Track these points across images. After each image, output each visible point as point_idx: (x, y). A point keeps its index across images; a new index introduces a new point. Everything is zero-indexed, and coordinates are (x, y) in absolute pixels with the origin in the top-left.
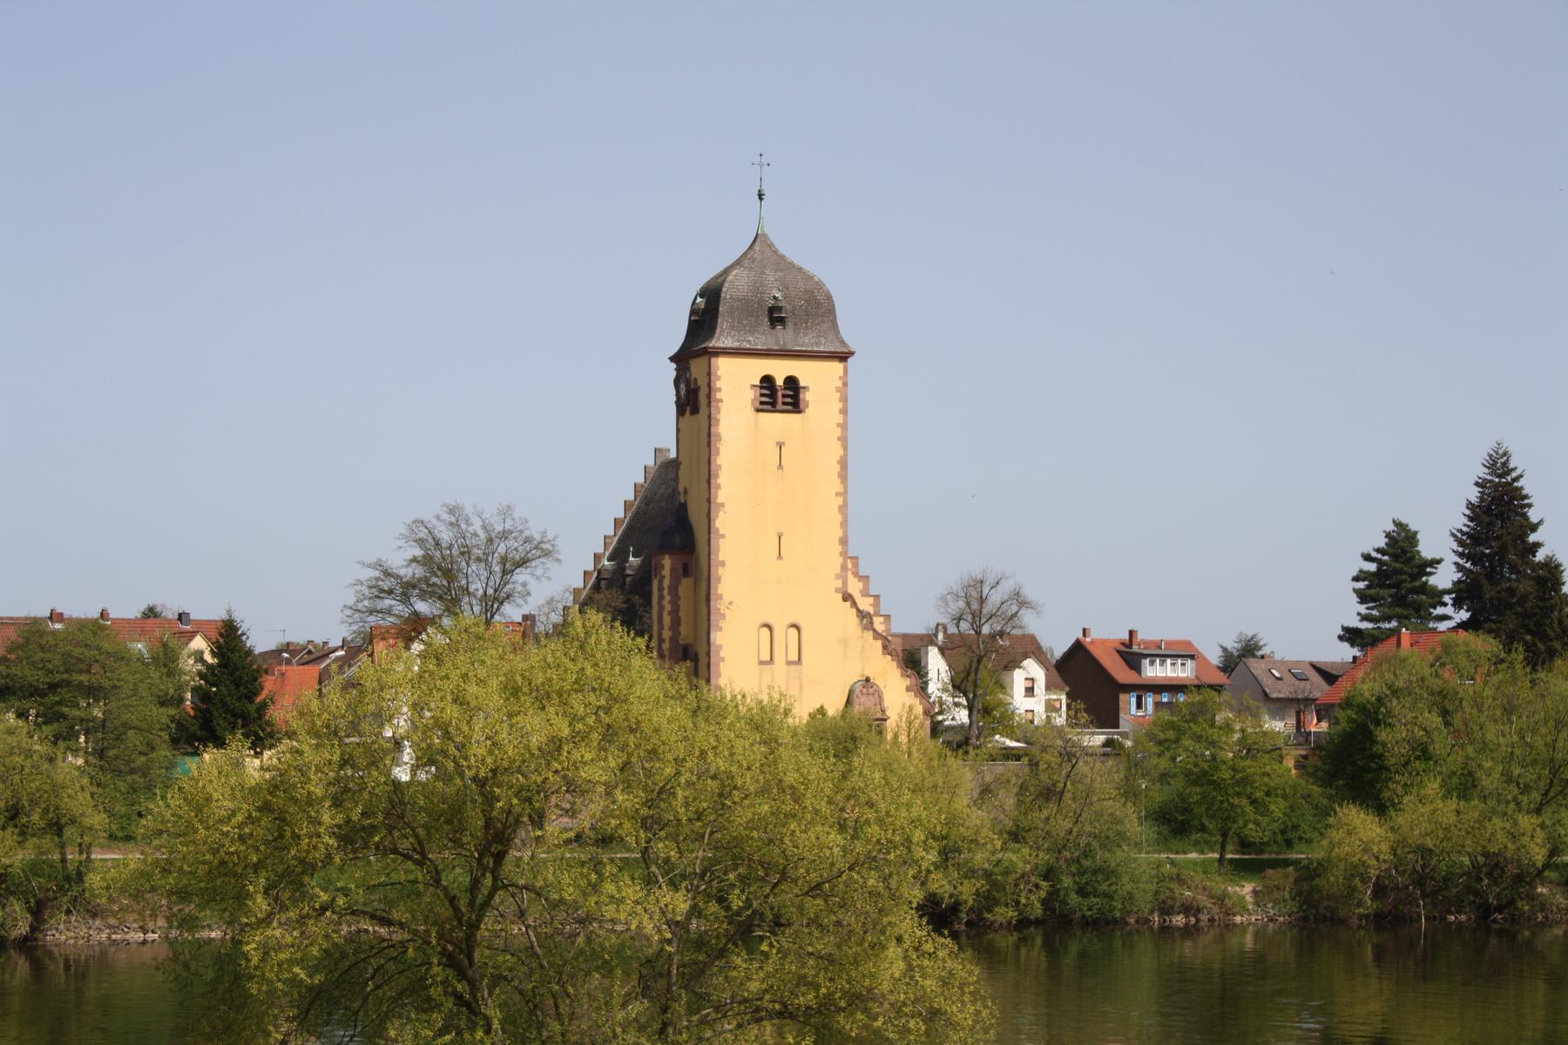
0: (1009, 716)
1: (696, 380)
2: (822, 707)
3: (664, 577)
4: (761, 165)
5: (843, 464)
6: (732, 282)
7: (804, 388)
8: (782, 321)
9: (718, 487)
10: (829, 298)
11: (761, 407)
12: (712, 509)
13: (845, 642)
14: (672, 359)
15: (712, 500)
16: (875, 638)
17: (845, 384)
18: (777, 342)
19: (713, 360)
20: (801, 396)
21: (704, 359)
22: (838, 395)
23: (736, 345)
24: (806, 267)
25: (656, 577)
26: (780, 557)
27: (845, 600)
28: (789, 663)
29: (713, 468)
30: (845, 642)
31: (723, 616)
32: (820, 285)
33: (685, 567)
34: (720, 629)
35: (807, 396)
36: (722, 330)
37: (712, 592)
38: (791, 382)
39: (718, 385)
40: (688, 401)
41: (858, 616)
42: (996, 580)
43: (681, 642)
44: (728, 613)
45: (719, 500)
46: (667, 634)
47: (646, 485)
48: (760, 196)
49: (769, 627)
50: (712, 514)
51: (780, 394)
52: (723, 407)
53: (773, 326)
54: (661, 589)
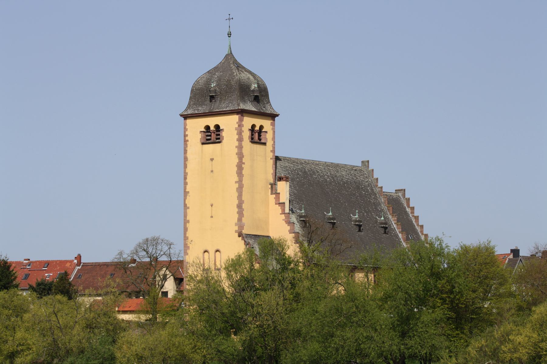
2: (378, 178)
22: (236, 132)
27: (239, 236)
35: (224, 134)
38: (217, 127)
41: (244, 244)
44: (190, 246)
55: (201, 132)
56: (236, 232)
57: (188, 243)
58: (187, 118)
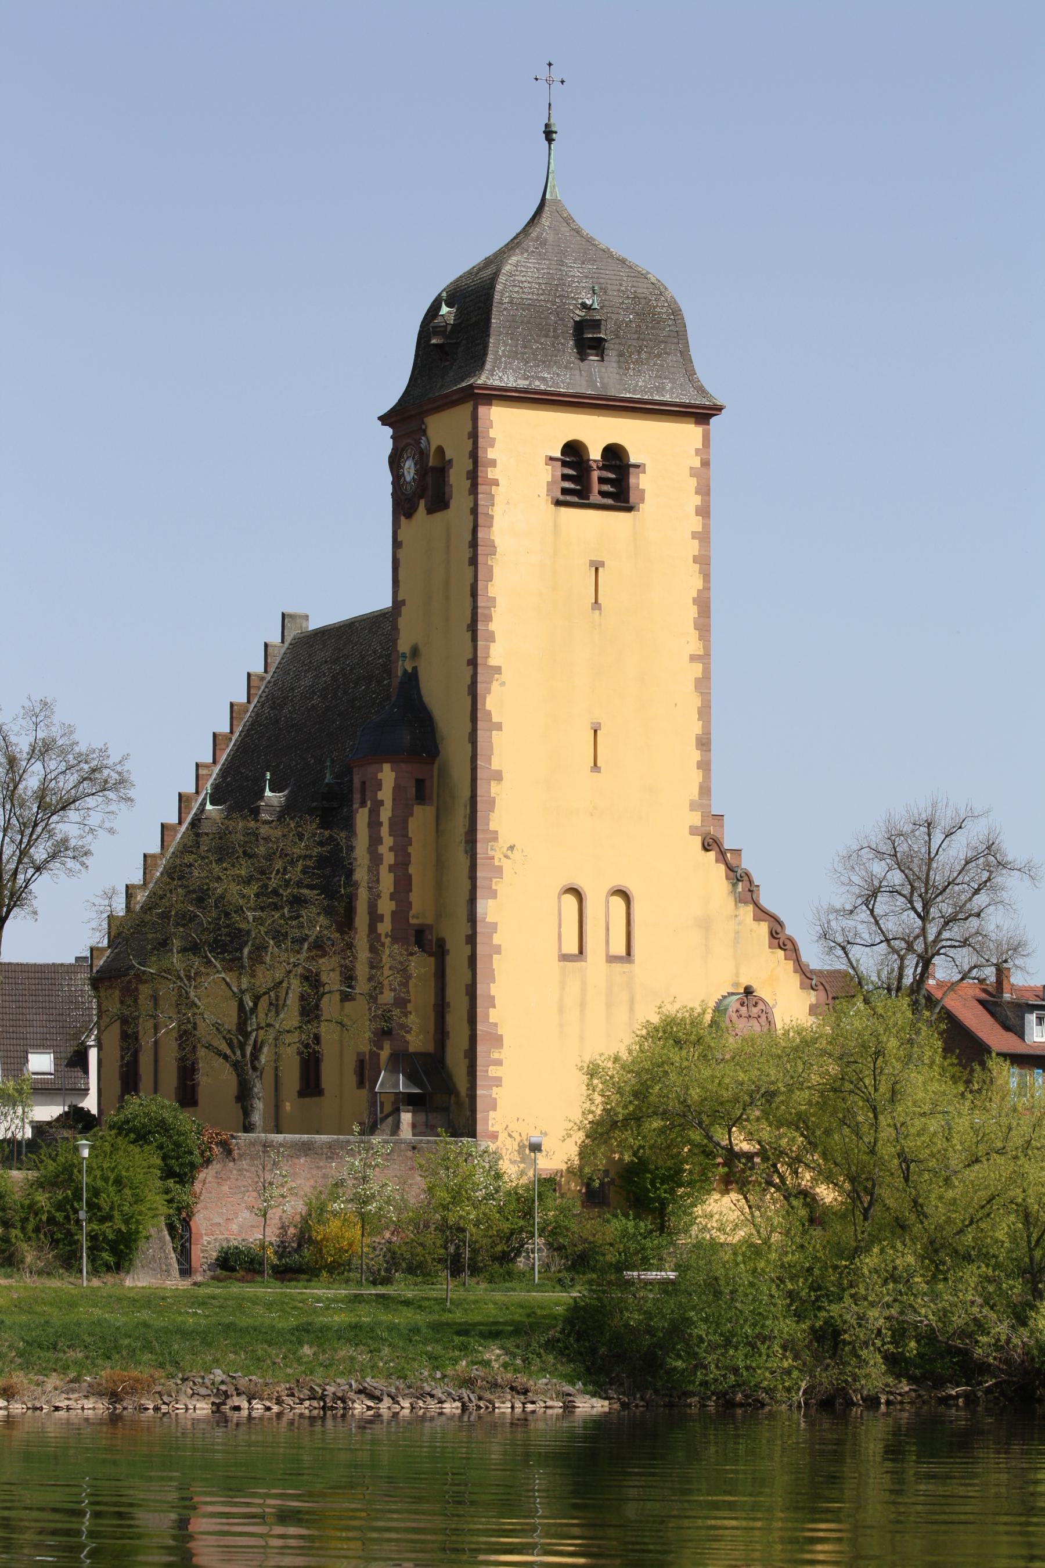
0: (970, 1060)
1: (440, 450)
3: (381, 803)
4: (549, 82)
5: (703, 604)
6: (511, 274)
7: (637, 466)
8: (598, 346)
9: (491, 637)
10: (676, 313)
11: (562, 498)
12: (480, 678)
13: (705, 925)
14: (385, 420)
15: (479, 661)
16: (756, 919)
17: (706, 463)
18: (591, 382)
19: (482, 410)
20: (632, 481)
21: (468, 407)
22: (693, 482)
23: (522, 384)
24: (632, 258)
25: (363, 804)
26: (595, 766)
27: (706, 848)
28: (612, 959)
29: (481, 603)
30: (705, 925)
31: (499, 870)
32: (657, 288)
33: (420, 784)
34: (494, 895)
35: (642, 482)
36: (497, 358)
37: (480, 826)
38: (614, 454)
39: (491, 454)
40: (421, 489)
41: (727, 878)
42: (958, 821)
43: (412, 921)
44: (506, 864)
45: (493, 662)
46: (386, 907)
47: (268, 677)
48: (549, 134)
49: (576, 892)
50: (480, 687)
51: (595, 475)
52: (500, 493)
53: (582, 356)
54: (374, 824)
55: (551, 459)
56: (693, 831)
57: (498, 855)
58: (494, 402)
